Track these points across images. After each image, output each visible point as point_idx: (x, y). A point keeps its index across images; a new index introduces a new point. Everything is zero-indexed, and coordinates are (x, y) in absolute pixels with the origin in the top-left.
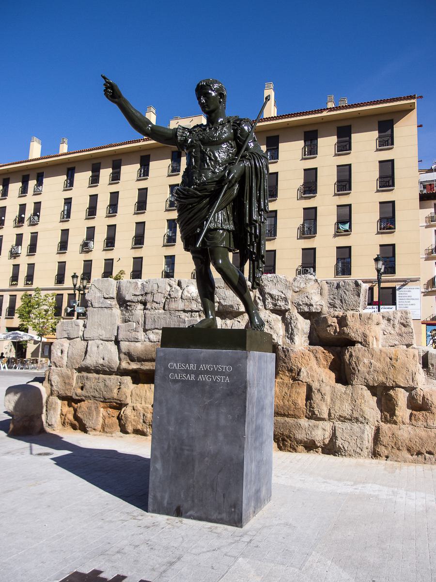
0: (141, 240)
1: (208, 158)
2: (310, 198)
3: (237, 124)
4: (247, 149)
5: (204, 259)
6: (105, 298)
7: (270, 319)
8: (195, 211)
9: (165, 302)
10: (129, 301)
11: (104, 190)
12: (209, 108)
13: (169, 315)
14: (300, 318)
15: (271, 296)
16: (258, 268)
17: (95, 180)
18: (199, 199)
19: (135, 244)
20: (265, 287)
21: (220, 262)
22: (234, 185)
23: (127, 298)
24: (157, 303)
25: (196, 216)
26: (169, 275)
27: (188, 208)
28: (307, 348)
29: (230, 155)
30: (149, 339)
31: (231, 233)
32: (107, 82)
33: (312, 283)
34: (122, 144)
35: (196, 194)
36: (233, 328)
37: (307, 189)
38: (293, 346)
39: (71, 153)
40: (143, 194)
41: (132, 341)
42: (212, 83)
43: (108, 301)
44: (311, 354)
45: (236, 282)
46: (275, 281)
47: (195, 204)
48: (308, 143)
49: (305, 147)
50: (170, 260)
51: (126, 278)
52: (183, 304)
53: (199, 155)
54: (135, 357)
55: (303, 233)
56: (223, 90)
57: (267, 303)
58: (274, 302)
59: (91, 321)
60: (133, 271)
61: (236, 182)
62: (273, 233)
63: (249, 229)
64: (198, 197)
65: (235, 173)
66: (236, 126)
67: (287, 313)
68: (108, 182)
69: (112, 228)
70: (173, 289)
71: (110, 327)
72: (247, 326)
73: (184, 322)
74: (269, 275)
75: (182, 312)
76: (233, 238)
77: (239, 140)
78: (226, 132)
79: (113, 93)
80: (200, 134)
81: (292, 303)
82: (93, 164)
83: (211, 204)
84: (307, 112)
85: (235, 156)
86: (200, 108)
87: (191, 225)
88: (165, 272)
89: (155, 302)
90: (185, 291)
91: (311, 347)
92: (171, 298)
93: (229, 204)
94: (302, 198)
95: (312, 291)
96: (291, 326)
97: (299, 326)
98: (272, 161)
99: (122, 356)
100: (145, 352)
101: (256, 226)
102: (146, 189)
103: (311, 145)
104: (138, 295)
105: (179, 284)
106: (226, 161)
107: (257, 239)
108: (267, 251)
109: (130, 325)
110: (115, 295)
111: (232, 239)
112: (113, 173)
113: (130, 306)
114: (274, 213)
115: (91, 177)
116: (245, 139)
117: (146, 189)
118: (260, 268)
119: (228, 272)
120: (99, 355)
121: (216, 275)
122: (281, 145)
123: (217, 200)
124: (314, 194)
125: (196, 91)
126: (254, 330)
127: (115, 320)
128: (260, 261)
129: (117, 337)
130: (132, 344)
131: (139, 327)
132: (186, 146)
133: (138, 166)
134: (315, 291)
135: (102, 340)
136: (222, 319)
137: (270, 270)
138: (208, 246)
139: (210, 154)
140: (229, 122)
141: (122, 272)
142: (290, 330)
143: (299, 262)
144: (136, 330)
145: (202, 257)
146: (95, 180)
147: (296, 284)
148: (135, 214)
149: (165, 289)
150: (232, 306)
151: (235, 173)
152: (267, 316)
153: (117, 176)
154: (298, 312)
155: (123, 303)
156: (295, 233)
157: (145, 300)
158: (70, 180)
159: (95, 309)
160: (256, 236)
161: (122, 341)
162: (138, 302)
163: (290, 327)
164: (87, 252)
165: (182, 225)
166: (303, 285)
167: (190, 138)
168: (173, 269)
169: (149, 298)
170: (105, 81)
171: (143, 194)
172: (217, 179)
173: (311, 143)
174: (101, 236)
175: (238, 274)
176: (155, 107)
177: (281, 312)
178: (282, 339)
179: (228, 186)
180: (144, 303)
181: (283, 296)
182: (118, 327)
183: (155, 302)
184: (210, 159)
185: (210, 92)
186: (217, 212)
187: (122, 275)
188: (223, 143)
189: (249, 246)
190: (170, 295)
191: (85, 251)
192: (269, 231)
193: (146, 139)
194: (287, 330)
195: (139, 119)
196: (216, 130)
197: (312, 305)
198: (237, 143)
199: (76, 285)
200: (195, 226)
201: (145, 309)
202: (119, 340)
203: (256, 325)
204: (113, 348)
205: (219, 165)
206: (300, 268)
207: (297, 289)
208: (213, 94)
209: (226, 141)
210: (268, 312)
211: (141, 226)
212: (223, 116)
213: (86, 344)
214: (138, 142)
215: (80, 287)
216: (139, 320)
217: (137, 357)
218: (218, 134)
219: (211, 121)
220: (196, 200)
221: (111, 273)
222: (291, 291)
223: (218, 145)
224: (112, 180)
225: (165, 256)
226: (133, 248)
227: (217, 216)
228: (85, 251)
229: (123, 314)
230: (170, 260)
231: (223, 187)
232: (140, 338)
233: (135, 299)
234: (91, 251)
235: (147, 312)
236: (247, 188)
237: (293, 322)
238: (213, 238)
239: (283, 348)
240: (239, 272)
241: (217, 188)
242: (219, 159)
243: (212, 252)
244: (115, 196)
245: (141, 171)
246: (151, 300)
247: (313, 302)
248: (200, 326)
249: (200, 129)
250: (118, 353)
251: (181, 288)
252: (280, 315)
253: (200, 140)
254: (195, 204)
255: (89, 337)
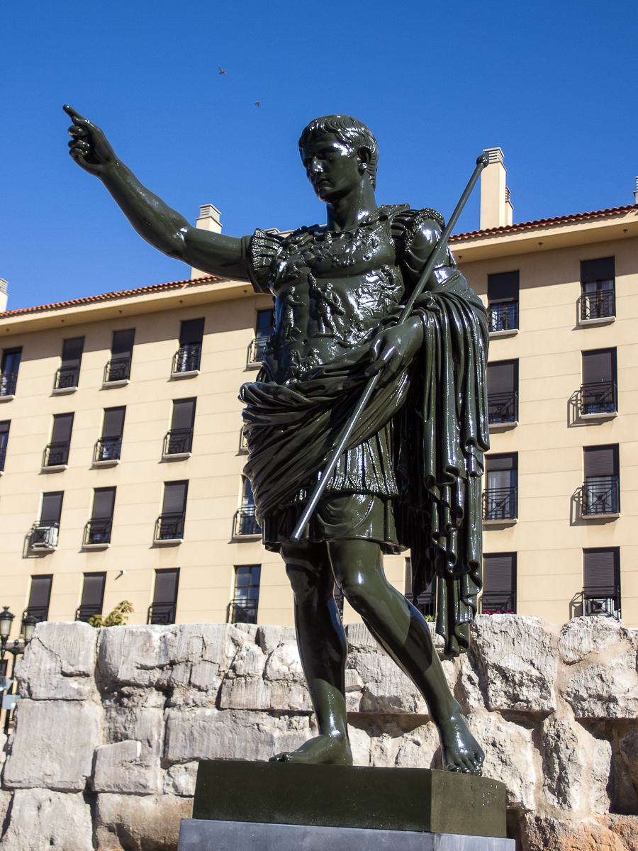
0: (176, 526)
1: (329, 309)
2: (600, 421)
3: (403, 224)
4: (430, 285)
5: (321, 577)
6: (64, 674)
7: (500, 737)
8: (294, 444)
9: (221, 688)
10: (127, 684)
11: (90, 401)
12: (333, 185)
13: (229, 723)
14: (584, 735)
15: (504, 674)
16: (463, 596)
17: (68, 379)
18: (304, 414)
19: (162, 536)
20: (486, 650)
21: (360, 580)
22: (394, 377)
23: (123, 675)
24: (200, 689)
25: (298, 456)
26: (245, 615)
27: (275, 436)
28: (604, 820)
29: (387, 300)
30: (175, 787)
31: (389, 502)
32: (77, 124)
33: (613, 638)
34: (136, 293)
35: (295, 400)
36: (403, 765)
37: (593, 399)
38: (566, 813)
39: (14, 315)
40: (185, 411)
41: (129, 794)
42: (340, 126)
43: (74, 684)
44: (617, 837)
45: (402, 636)
46: (512, 633)
47: (294, 427)
48: (592, 288)
49: (583, 297)
50: (249, 577)
51: (137, 620)
52: (268, 693)
53: (306, 301)
54: (136, 836)
55: (585, 509)
56: (368, 142)
57: (491, 693)
58: (511, 690)
59: (24, 736)
60: (154, 605)
61: (401, 368)
62: (507, 509)
63: (436, 493)
64: (302, 407)
65: (399, 347)
66: (402, 229)
67: (547, 722)
68: (100, 383)
69: (106, 495)
70: (244, 653)
71: (73, 754)
72: (436, 762)
73: (271, 742)
74: (497, 617)
75: (265, 715)
76: (395, 515)
77: (409, 262)
78: (378, 244)
79: (92, 149)
80: (311, 250)
81: (561, 692)
82: (66, 341)
83: (337, 425)
84: (586, 214)
85: (400, 304)
86: (312, 185)
87: (282, 480)
88: (237, 608)
89: (195, 686)
90: (274, 658)
91: (618, 819)
92: (238, 676)
93: (383, 425)
94: (579, 422)
95: (614, 662)
96: (559, 758)
97: (581, 758)
98: (503, 332)
99: (103, 834)
100: (164, 825)
101: (456, 483)
102: (194, 400)
103: (598, 294)
104: (152, 668)
105: (260, 639)
106: (376, 316)
107: (458, 519)
108: (487, 556)
109: (126, 750)
110: (90, 666)
111: (391, 519)
112: (112, 363)
113: (129, 696)
114: (510, 460)
115: (61, 370)
116: (425, 261)
117: (194, 400)
118: (469, 596)
119: (382, 608)
120: (41, 831)
121: (350, 617)
122: (524, 294)
123: (351, 415)
124: (609, 411)
125: (300, 145)
126: (454, 770)
127: (89, 734)
128: (468, 578)
129: (90, 782)
130: (131, 800)
131: (149, 753)
132: (273, 279)
133: (174, 345)
134: (621, 661)
135: (53, 789)
136: (372, 734)
137: (501, 604)
138: (328, 537)
139: (335, 299)
140: (383, 218)
141: (124, 607)
142: (557, 769)
143: (578, 584)
144: (141, 763)
145: (310, 567)
146: (68, 379)
147: (569, 641)
148: (165, 460)
149: (222, 652)
150: (397, 701)
151: (400, 342)
152: (492, 729)
153: (124, 370)
154: (577, 719)
155: (112, 688)
156: (564, 509)
157: (169, 681)
158: (9, 377)
159: (37, 703)
160: (456, 512)
161: (103, 791)
162: (150, 685)
163: (557, 761)
164: (42, 554)
165: (260, 480)
166: (587, 645)
167: (284, 260)
168: (254, 600)
169: (180, 674)
170: (73, 120)
171: (185, 411)
172: (353, 362)
173: (599, 287)
174: (77, 514)
175: (408, 614)
176: (219, 208)
177: (531, 719)
178: (536, 792)
179: (379, 380)
180: (167, 690)
181: (535, 673)
182: (95, 755)
183: (195, 686)
184: (335, 311)
185: (336, 145)
186: (351, 446)
187: (125, 614)
188: (368, 271)
189: (437, 536)
190: (233, 668)
191: (36, 553)
192: (498, 504)
193: (206, 279)
194: (548, 769)
195: (154, 212)
196: (351, 238)
197: (614, 700)
198: (405, 272)
199: (7, 639)
200: (296, 482)
201: (167, 705)
202: (97, 789)
203: (457, 759)
204: (78, 809)
205: (357, 325)
206: (580, 599)
207: (572, 656)
208: (345, 151)
209: (376, 265)
210: (494, 717)
211: (177, 489)
212: (370, 205)
213: (10, 797)
214: (175, 288)
215: (16, 643)
216: (152, 735)
217: (142, 839)
218: (354, 248)
219: (340, 216)
220: (298, 415)
221: (99, 609)
222: (557, 659)
223: (357, 274)
224: (111, 379)
225: (237, 567)
226: (156, 546)
227: (352, 459)
228: (36, 553)
229: (110, 719)
230: (249, 577)
231: (367, 380)
232: (151, 784)
233: (144, 678)
234: (52, 552)
235: (172, 712)
236: (431, 384)
237: (562, 746)
238: (340, 516)
239: (538, 819)
240: (409, 607)
241: (353, 384)
242: (359, 312)
243: (338, 553)
244: (115, 416)
245: (181, 358)
246: (186, 681)
247: (616, 691)
248: (304, 759)
249: (310, 237)
250: (90, 825)
251: (264, 650)
252: (527, 726)
253: (309, 264)
254: (294, 427)
255: (16, 778)
